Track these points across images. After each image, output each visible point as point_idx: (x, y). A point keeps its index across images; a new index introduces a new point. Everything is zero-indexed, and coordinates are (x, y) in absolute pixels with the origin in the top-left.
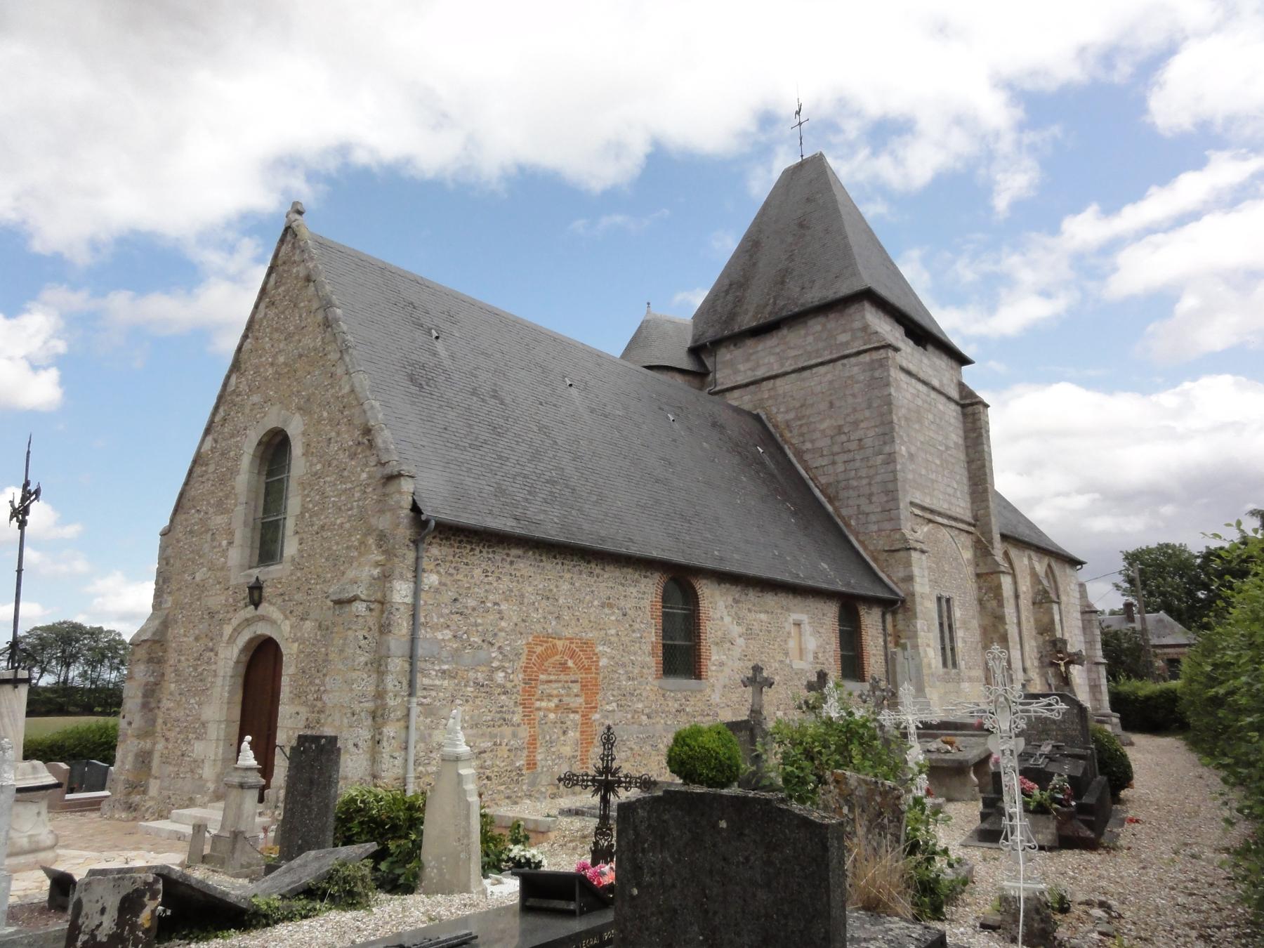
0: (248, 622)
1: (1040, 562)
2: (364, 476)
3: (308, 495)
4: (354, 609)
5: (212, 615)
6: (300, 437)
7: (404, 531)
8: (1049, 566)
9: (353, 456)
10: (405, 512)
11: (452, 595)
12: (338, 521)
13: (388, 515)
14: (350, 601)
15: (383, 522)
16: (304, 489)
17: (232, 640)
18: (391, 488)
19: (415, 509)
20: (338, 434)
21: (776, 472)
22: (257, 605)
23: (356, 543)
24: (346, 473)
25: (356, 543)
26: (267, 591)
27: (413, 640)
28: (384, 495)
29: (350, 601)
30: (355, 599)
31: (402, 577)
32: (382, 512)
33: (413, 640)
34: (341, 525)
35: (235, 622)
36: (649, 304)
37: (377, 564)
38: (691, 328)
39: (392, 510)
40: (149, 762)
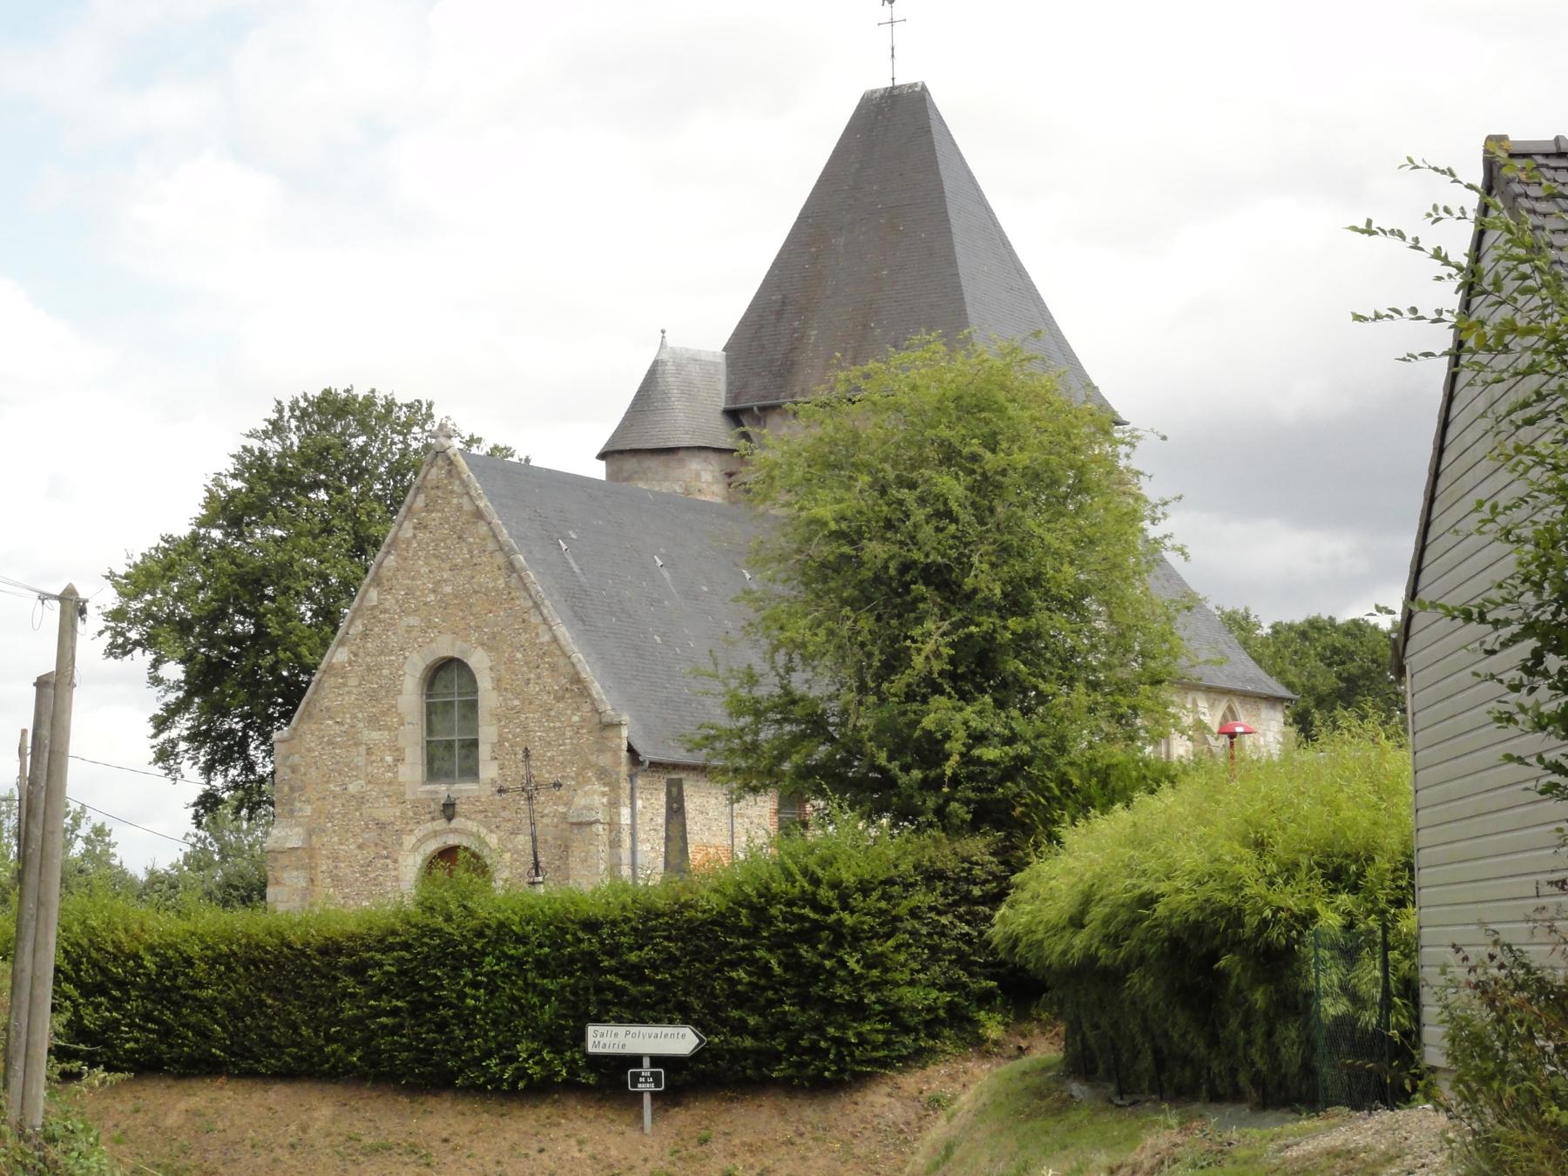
0: (435, 834)
1: (1212, 706)
2: (576, 719)
3: (505, 727)
4: (594, 829)
5: (381, 826)
6: (488, 671)
7: (624, 768)
8: (1230, 709)
9: (559, 699)
10: (624, 754)
11: (649, 815)
12: (549, 754)
13: (609, 755)
14: (590, 824)
15: (605, 760)
16: (500, 721)
17: (415, 849)
18: (609, 733)
19: (631, 749)
20: (539, 677)
21: (1294, 1152)
22: (450, 819)
23: (573, 774)
24: (553, 713)
25: (573, 774)
26: (461, 808)
27: (633, 852)
28: (602, 738)
29: (590, 824)
30: (597, 821)
31: (625, 805)
32: (601, 751)
33: (633, 852)
34: (552, 758)
35: (418, 833)
36: (663, 332)
37: (604, 794)
38: (723, 368)
39: (611, 749)
40: (591, 926)
